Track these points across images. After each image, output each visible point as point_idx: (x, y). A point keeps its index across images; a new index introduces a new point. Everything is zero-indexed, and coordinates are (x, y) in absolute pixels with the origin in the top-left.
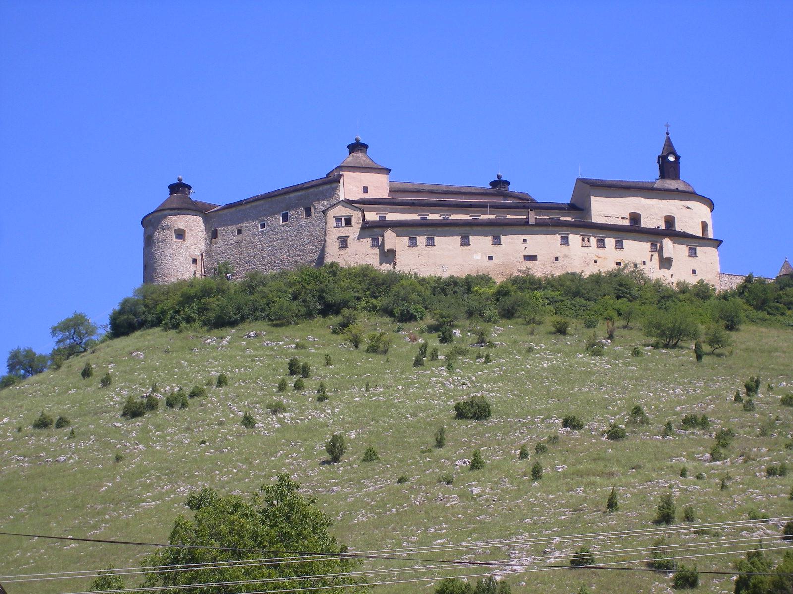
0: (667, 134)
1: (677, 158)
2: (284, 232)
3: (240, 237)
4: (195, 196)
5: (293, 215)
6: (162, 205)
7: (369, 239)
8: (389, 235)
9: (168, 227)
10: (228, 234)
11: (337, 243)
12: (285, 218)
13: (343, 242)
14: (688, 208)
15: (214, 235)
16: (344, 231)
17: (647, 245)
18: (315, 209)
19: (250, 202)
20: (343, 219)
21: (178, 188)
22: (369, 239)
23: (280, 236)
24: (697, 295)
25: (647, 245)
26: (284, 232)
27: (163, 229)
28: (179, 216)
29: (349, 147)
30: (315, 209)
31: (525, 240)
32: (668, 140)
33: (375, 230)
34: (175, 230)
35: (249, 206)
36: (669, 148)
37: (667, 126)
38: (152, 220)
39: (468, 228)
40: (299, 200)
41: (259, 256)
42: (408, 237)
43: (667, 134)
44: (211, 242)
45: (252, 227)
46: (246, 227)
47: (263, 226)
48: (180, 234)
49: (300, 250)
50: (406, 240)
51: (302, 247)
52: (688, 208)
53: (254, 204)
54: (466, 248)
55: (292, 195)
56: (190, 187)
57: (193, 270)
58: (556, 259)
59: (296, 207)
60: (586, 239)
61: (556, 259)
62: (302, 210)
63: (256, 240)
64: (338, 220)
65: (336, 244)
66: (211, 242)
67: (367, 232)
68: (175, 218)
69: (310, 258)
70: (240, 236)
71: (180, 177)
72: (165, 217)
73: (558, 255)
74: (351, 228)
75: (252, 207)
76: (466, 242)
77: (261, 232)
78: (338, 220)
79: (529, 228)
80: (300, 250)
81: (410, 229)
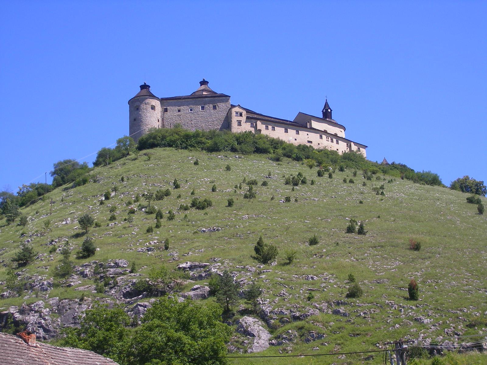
0: (326, 100)
1: (331, 110)
2: (202, 114)
3: (179, 113)
4: (152, 90)
5: (207, 107)
6: (139, 93)
7: (250, 123)
8: (259, 123)
9: (148, 104)
10: (173, 110)
11: (237, 123)
12: (203, 108)
13: (239, 123)
14: (341, 131)
15: (166, 110)
16: (240, 118)
17: (346, 144)
18: (218, 106)
19: (186, 98)
20: (239, 113)
21: (144, 87)
22: (250, 123)
23: (200, 116)
24: (64, 163)
25: (346, 144)
26: (202, 114)
27: (146, 104)
28: (152, 99)
29: (200, 83)
30: (218, 106)
31: (308, 134)
32: (326, 103)
33: (252, 120)
34: (151, 105)
35: (184, 100)
36: (326, 105)
37: (326, 97)
38: (139, 99)
39: (287, 126)
40: (210, 102)
41: (189, 123)
42: (265, 125)
43: (326, 100)
44: (164, 113)
45: (185, 109)
46: (183, 109)
47: (191, 110)
48: (153, 108)
49: (211, 123)
50: (264, 126)
51: (212, 122)
52: (341, 131)
53: (186, 100)
54: (286, 133)
55: (206, 99)
56: (149, 87)
57: (158, 124)
58: (319, 144)
59: (209, 103)
60: (327, 138)
61: (319, 144)
62: (211, 106)
63: (188, 115)
64: (237, 113)
65: (237, 123)
66: (164, 113)
67: (249, 120)
68: (151, 100)
69: (216, 128)
70: (180, 113)
71: (145, 82)
72: (147, 99)
73: (319, 143)
74: (242, 117)
75: (185, 101)
76: (286, 131)
77: (191, 112)
78: (237, 113)
79: (307, 129)
80: (211, 123)
81: (266, 122)
